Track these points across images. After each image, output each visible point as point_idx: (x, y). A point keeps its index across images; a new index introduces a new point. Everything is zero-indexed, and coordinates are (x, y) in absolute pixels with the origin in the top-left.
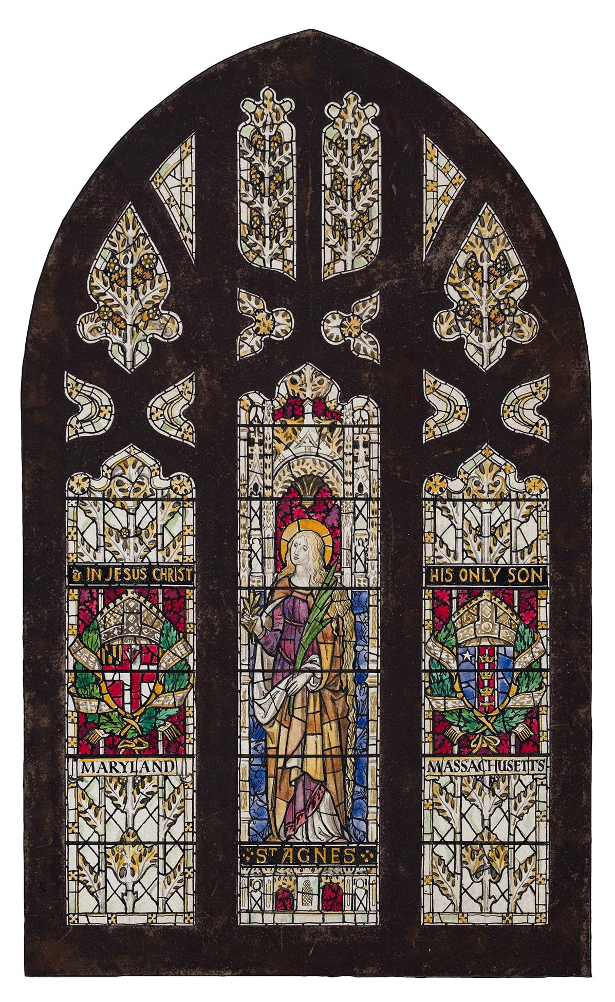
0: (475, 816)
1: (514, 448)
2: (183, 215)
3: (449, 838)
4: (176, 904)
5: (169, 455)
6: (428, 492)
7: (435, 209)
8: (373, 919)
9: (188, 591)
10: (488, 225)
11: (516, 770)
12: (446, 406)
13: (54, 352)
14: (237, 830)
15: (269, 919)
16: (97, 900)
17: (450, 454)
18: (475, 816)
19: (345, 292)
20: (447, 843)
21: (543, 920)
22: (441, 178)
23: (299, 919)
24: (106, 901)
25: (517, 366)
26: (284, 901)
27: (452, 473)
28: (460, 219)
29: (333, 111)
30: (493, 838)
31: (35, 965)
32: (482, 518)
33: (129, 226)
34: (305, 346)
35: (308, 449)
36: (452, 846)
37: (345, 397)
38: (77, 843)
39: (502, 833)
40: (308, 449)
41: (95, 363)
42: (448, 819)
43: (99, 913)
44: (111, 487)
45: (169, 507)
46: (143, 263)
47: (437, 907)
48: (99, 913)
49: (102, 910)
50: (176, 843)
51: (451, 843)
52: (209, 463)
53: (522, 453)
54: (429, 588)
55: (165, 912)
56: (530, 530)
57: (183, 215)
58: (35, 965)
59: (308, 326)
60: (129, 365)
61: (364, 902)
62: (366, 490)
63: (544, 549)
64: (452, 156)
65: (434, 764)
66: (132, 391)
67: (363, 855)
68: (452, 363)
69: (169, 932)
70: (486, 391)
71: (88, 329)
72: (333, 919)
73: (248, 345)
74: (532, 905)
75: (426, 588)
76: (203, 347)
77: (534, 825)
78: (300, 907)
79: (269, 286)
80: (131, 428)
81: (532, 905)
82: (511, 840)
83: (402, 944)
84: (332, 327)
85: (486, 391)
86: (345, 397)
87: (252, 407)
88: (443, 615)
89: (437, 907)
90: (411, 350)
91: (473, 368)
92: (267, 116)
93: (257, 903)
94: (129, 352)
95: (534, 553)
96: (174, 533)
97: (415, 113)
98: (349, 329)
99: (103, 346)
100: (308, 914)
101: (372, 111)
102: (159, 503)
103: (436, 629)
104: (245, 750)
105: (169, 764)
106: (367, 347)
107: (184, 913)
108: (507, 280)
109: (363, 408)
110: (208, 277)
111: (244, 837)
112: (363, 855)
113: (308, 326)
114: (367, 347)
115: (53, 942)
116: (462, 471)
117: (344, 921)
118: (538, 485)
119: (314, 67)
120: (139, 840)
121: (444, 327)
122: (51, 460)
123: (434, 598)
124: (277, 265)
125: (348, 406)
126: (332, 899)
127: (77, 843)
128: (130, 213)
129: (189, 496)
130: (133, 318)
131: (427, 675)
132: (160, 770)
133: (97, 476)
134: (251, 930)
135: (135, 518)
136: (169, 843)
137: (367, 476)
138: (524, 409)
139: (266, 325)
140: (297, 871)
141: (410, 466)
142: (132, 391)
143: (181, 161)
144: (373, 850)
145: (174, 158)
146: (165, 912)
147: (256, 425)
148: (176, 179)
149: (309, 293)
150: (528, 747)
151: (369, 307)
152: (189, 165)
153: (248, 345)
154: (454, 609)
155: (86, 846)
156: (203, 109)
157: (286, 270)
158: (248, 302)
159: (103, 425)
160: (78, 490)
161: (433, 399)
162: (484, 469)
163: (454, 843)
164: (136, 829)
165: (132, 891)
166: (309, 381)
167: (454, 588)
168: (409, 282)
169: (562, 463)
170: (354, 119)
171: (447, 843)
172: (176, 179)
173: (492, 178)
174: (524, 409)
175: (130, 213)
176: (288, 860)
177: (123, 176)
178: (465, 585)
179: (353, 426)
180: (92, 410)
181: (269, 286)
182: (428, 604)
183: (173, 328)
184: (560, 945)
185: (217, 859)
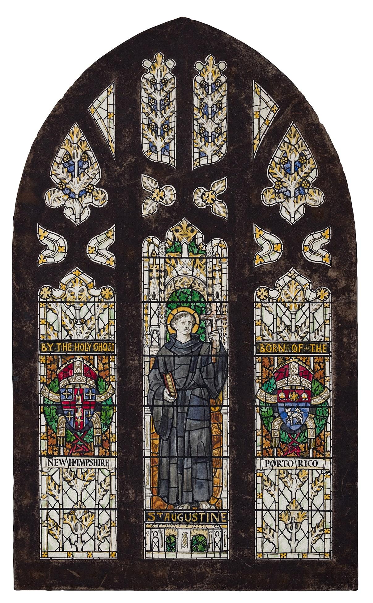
0: (73, 494)
1: (312, 270)
5: (100, 275)
6: (258, 298)
7: (259, 128)
9: (326, 358)
10: (294, 137)
11: (55, 465)
12: (268, 247)
13: (31, 212)
15: (162, 556)
16: (273, 544)
18: (73, 494)
20: (55, 509)
22: (264, 109)
23: (180, 556)
24: (63, 544)
25: (312, 220)
26: (171, 545)
27: (55, 285)
28: (275, 134)
29: (199, 66)
30: (84, 507)
31: (350, 583)
33: (74, 140)
34: (184, 208)
36: (58, 511)
37: (207, 240)
39: (90, 504)
41: (56, 220)
42: (272, 495)
43: (59, 551)
44: (281, 296)
45: (102, 306)
46: (302, 162)
47: (263, 548)
48: (275, 553)
49: (61, 550)
52: (123, 281)
54: (259, 356)
55: (312, 552)
56: (105, 317)
58: (350, 583)
59: (185, 196)
60: (78, 221)
62: (157, 297)
63: (113, 330)
64: (270, 93)
65: (82, 461)
66: (78, 237)
68: (272, 220)
69: (102, 563)
70: (292, 236)
71: (53, 199)
73: (149, 208)
75: (256, 356)
77: (322, 500)
78: (180, 549)
79: (161, 173)
80: (77, 258)
81: (323, 547)
82: (310, 508)
83: (244, 570)
84: (200, 198)
85: (292, 236)
86: (207, 240)
89: (263, 548)
90: (247, 213)
91: (284, 222)
92: (159, 68)
94: (77, 212)
95: (106, 332)
96: (103, 321)
97: (247, 68)
98: (211, 198)
100: (184, 553)
101: (171, 64)
102: (96, 304)
104: (147, 454)
106: (220, 209)
107: (110, 551)
108: (304, 169)
109: (218, 247)
110: (123, 167)
113: (185, 196)
114: (220, 209)
115: (31, 570)
116: (278, 285)
117: (220, 557)
118: (108, 291)
119: (185, 40)
120: (83, 503)
121: (268, 198)
122: (30, 279)
124: (166, 160)
125: (210, 245)
126: (198, 544)
127: (262, 510)
128: (76, 128)
129: (328, 301)
130: (77, 193)
131: (258, 408)
132: (52, 465)
133: (57, 287)
134: (153, 561)
135: (80, 311)
137: (221, 286)
139: (158, 196)
140: (177, 526)
141: (247, 280)
142: (78, 237)
143: (108, 96)
145: (105, 94)
146: (312, 552)
147: (154, 256)
148: (104, 108)
149: (185, 177)
151: (220, 186)
152: (112, 100)
153: (149, 208)
155: (318, 512)
156: (120, 67)
157: (195, 162)
158: (148, 182)
159: (60, 257)
160: (46, 296)
161: (260, 241)
162: (293, 285)
163: (60, 509)
164: (83, 501)
166: (184, 232)
167: (96, 355)
168: (245, 169)
170: (210, 70)
171: (55, 509)
172: (104, 108)
173: (294, 107)
174: (316, 246)
175: (76, 128)
177: (73, 108)
179: (213, 258)
180: (54, 248)
181: (161, 173)
182: (258, 366)
183: (101, 199)
184: (341, 570)
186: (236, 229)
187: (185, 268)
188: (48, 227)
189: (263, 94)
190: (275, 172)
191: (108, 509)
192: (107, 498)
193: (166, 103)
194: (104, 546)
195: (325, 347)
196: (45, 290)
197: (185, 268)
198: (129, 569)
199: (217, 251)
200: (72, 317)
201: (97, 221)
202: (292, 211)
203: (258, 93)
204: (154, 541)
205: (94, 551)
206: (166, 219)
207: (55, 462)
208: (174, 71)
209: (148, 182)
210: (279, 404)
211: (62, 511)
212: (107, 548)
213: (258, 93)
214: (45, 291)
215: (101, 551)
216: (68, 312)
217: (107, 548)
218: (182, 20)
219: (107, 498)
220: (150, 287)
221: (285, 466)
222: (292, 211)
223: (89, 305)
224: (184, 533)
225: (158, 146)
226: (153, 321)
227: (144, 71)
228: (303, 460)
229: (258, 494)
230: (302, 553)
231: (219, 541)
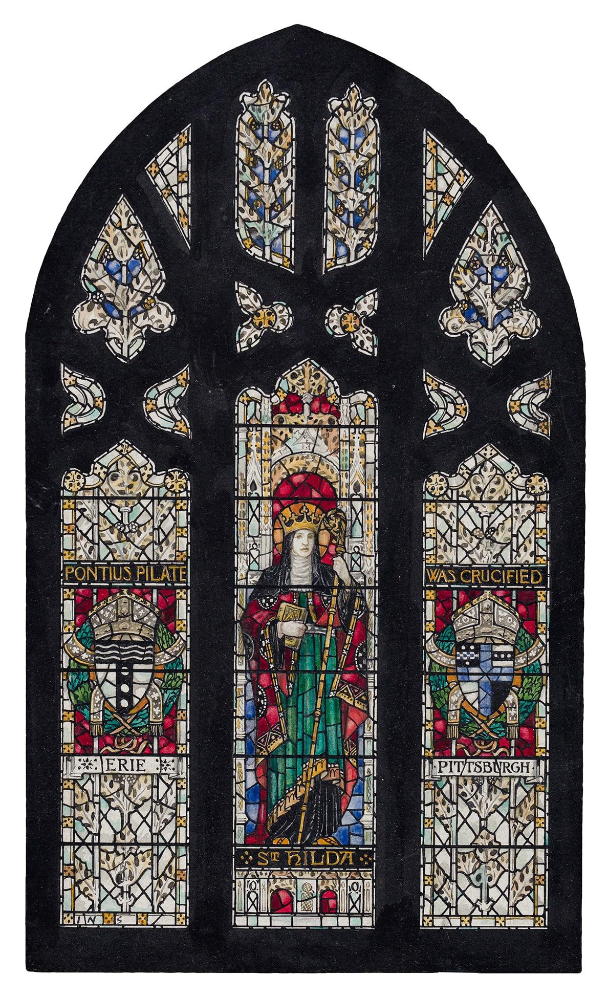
2: (179, 207)
3: (89, 840)
4: (526, 906)
5: (163, 450)
7: (435, 211)
8: (368, 922)
12: (448, 410)
14: (231, 831)
15: (264, 921)
17: (452, 451)
19: (345, 287)
20: (87, 845)
21: (66, 921)
22: (444, 176)
23: (301, 922)
25: (522, 361)
32: (480, 515)
33: (122, 233)
35: (304, 447)
38: (73, 844)
40: (304, 447)
41: (92, 355)
45: (168, 504)
50: (443, 846)
51: (89, 844)
52: (204, 460)
53: (523, 450)
57: (179, 207)
58: (574, 966)
61: (250, 903)
62: (362, 492)
66: (125, 384)
67: (361, 859)
68: (456, 361)
71: (85, 318)
72: (329, 921)
73: (247, 337)
74: (528, 913)
76: (202, 342)
83: (399, 941)
84: (334, 320)
85: (488, 388)
87: (253, 404)
88: (83, 608)
92: (264, 107)
93: (253, 903)
94: (126, 343)
97: (412, 110)
98: (353, 323)
99: (102, 336)
103: (438, 631)
105: (135, 763)
106: (366, 342)
107: (176, 913)
109: (361, 405)
110: (202, 267)
111: (240, 839)
112: (361, 859)
114: (366, 342)
115: (51, 943)
119: (307, 63)
121: (452, 321)
122: (52, 454)
123: (437, 601)
130: (128, 310)
135: (133, 511)
136: (438, 847)
138: (526, 405)
139: (261, 318)
141: (409, 462)
144: (370, 853)
150: (526, 749)
151: (367, 303)
153: (247, 337)
154: (95, 603)
156: (200, 105)
158: (247, 298)
163: (93, 844)
165: (129, 892)
166: (307, 378)
168: (411, 270)
169: (558, 459)
171: (87, 845)
173: (491, 178)
174: (526, 405)
176: (294, 860)
177: (118, 173)
178: (467, 584)
182: (430, 605)
184: (557, 947)
185: (211, 859)
186: (394, 376)
187: (309, 439)
188: (76, 365)
189: (444, 155)
190: (463, 282)
191: (162, 844)
192: (171, 828)
193: (279, 205)
194: (526, 906)
195: (511, 573)
196: (435, 478)
197: (309, 439)
198: (209, 941)
199: (255, 414)
200: (114, 521)
201: (159, 357)
202: (490, 346)
203: (181, 144)
204: (252, 900)
205: (508, 915)
206: (272, 358)
207: (138, 764)
208: (292, 110)
209: (247, 298)
210: (99, 666)
211: (454, 850)
212: (172, 911)
213: (181, 144)
214: (435, 482)
215: (521, 915)
216: (108, 514)
217: (172, 911)
218: (298, 30)
219: (171, 828)
220: (253, 470)
221: (132, 770)
222: (490, 346)
223: (145, 502)
224: (307, 884)
225: (268, 236)
226: (254, 544)
227: (240, 111)
228: (128, 758)
229: (426, 820)
230: (482, 916)
231: (358, 902)
